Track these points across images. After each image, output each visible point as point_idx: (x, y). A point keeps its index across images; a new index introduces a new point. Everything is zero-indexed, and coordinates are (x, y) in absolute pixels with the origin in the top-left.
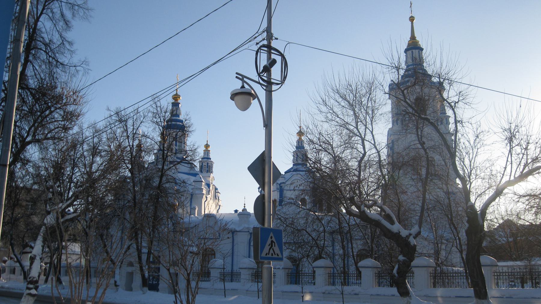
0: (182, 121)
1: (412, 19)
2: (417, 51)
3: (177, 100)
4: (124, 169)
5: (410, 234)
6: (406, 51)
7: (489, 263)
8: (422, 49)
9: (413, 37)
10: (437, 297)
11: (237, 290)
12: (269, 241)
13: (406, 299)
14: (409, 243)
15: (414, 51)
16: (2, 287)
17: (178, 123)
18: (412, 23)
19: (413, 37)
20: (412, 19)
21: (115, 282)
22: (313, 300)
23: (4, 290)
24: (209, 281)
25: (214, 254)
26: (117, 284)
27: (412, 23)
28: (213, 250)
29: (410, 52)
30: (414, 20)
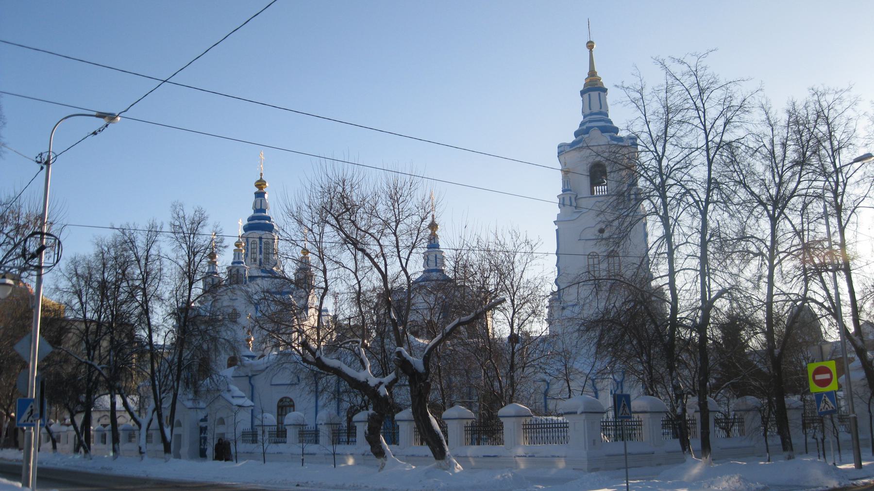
0: (269, 219)
1: (590, 45)
2: (596, 93)
3: (261, 188)
4: (814, 172)
5: (381, 383)
6: (582, 93)
7: (513, 413)
8: (605, 90)
9: (592, 73)
10: (466, 457)
11: (314, 454)
12: (29, 410)
13: (380, 461)
14: (378, 393)
15: (592, 93)
16: (2, 458)
17: (263, 221)
18: (591, 51)
19: (592, 73)
20: (590, 45)
21: (140, 448)
22: (357, 463)
23: (6, 462)
24: (285, 443)
25: (293, 406)
26: (142, 450)
27: (591, 51)
28: (291, 400)
29: (586, 96)
30: (593, 47)
